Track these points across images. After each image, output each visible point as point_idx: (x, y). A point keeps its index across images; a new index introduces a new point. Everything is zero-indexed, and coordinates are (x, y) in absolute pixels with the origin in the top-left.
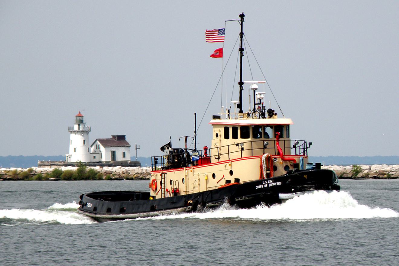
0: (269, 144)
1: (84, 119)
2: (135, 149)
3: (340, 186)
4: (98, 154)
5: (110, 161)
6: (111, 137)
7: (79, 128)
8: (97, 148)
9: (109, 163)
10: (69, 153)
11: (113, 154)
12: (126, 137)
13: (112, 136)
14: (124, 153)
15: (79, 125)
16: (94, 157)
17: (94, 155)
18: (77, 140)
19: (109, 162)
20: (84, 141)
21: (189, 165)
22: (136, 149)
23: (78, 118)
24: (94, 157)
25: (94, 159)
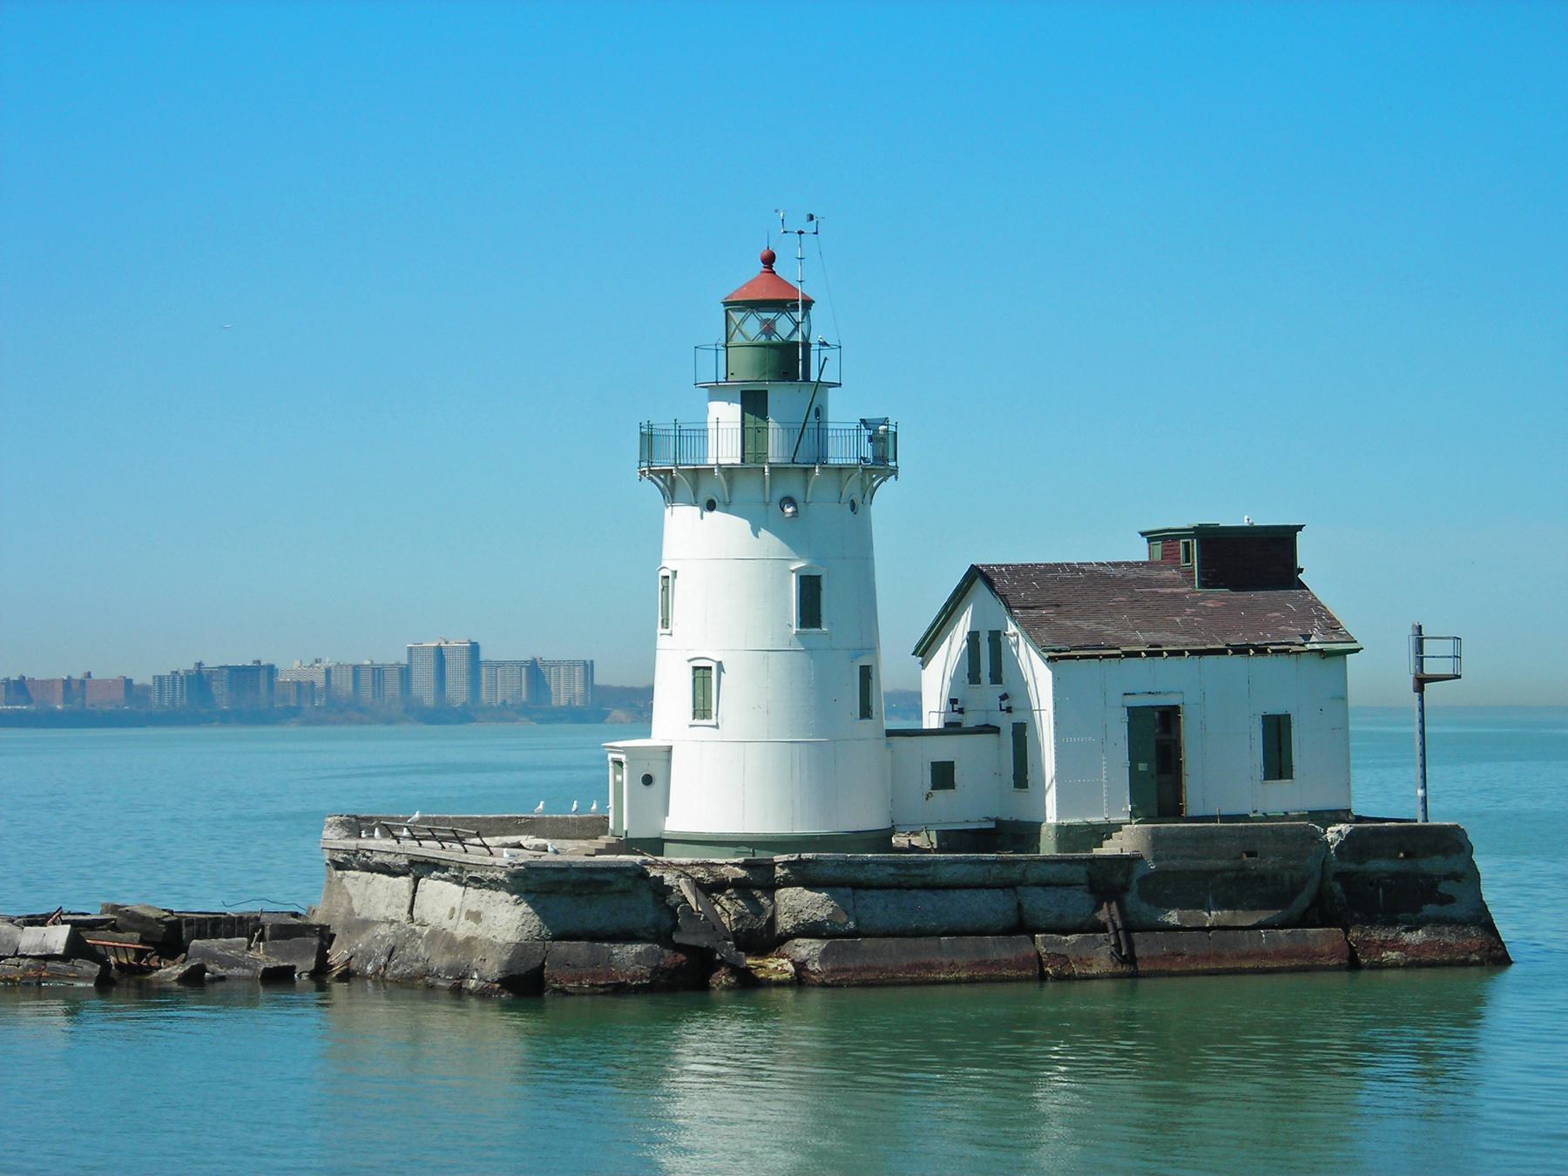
0: (906, 456)
1: (820, 326)
2: (1410, 682)
3: (1449, 842)
4: (992, 737)
5: (1118, 827)
6: (1139, 551)
7: (751, 439)
8: (974, 677)
9: (1109, 848)
10: (648, 735)
11: (1158, 741)
12: (1307, 554)
13: (1151, 536)
14: (1277, 731)
15: (754, 403)
16: (943, 775)
17: (945, 749)
18: (716, 580)
19: (1102, 832)
20: (810, 588)
21: (616, 713)
22: (1421, 682)
23: (752, 326)
24: (943, 775)
25: (940, 795)
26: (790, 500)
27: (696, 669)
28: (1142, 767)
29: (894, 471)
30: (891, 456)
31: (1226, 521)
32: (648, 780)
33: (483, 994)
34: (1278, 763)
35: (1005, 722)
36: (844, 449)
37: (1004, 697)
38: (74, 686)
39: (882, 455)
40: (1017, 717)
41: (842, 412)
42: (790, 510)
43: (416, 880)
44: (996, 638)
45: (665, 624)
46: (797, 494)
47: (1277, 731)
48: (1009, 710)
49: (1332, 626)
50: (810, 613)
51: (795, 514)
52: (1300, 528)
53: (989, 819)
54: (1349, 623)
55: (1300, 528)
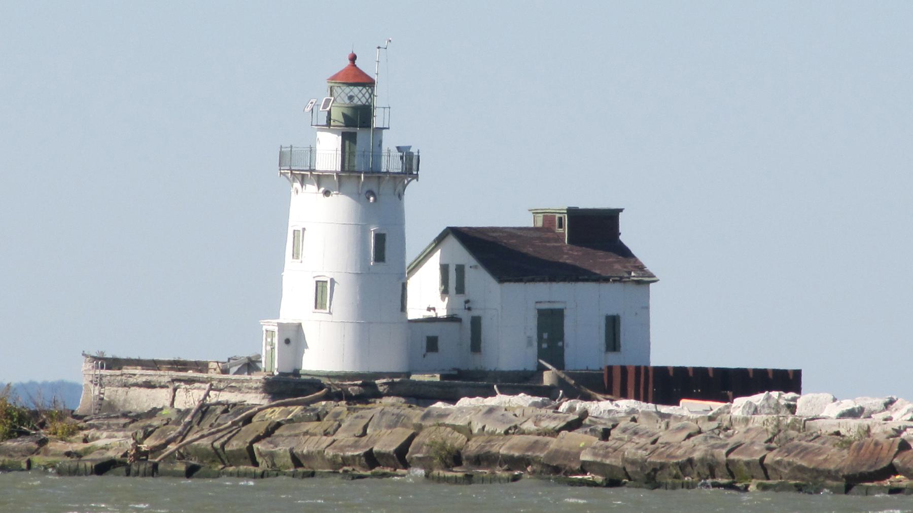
14: (613, 324)
18: (321, 227)
20: (380, 239)
25: (431, 355)
26: (371, 193)
27: (317, 282)
28: (560, 344)
29: (416, 177)
30: (415, 167)
31: (582, 206)
32: (287, 341)
33: (92, 473)
34: (613, 342)
35: (466, 317)
36: (391, 163)
37: (467, 302)
38: (584, 306)
39: (410, 165)
40: (475, 313)
41: (390, 142)
42: (372, 198)
43: (175, 390)
44: (460, 269)
45: (296, 255)
46: (375, 191)
47: (613, 324)
48: (469, 309)
49: (641, 268)
50: (380, 256)
51: (375, 200)
52: (621, 210)
53: (455, 369)
54: (650, 266)
55: (621, 210)
